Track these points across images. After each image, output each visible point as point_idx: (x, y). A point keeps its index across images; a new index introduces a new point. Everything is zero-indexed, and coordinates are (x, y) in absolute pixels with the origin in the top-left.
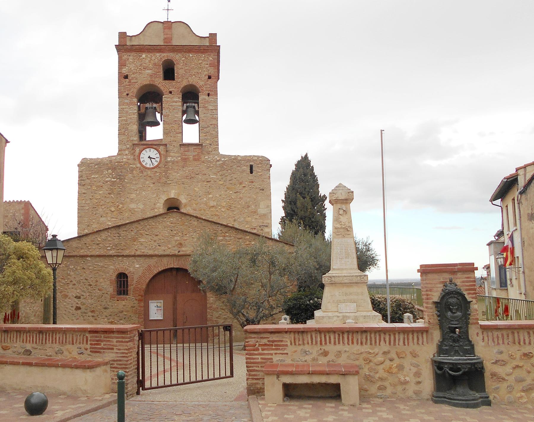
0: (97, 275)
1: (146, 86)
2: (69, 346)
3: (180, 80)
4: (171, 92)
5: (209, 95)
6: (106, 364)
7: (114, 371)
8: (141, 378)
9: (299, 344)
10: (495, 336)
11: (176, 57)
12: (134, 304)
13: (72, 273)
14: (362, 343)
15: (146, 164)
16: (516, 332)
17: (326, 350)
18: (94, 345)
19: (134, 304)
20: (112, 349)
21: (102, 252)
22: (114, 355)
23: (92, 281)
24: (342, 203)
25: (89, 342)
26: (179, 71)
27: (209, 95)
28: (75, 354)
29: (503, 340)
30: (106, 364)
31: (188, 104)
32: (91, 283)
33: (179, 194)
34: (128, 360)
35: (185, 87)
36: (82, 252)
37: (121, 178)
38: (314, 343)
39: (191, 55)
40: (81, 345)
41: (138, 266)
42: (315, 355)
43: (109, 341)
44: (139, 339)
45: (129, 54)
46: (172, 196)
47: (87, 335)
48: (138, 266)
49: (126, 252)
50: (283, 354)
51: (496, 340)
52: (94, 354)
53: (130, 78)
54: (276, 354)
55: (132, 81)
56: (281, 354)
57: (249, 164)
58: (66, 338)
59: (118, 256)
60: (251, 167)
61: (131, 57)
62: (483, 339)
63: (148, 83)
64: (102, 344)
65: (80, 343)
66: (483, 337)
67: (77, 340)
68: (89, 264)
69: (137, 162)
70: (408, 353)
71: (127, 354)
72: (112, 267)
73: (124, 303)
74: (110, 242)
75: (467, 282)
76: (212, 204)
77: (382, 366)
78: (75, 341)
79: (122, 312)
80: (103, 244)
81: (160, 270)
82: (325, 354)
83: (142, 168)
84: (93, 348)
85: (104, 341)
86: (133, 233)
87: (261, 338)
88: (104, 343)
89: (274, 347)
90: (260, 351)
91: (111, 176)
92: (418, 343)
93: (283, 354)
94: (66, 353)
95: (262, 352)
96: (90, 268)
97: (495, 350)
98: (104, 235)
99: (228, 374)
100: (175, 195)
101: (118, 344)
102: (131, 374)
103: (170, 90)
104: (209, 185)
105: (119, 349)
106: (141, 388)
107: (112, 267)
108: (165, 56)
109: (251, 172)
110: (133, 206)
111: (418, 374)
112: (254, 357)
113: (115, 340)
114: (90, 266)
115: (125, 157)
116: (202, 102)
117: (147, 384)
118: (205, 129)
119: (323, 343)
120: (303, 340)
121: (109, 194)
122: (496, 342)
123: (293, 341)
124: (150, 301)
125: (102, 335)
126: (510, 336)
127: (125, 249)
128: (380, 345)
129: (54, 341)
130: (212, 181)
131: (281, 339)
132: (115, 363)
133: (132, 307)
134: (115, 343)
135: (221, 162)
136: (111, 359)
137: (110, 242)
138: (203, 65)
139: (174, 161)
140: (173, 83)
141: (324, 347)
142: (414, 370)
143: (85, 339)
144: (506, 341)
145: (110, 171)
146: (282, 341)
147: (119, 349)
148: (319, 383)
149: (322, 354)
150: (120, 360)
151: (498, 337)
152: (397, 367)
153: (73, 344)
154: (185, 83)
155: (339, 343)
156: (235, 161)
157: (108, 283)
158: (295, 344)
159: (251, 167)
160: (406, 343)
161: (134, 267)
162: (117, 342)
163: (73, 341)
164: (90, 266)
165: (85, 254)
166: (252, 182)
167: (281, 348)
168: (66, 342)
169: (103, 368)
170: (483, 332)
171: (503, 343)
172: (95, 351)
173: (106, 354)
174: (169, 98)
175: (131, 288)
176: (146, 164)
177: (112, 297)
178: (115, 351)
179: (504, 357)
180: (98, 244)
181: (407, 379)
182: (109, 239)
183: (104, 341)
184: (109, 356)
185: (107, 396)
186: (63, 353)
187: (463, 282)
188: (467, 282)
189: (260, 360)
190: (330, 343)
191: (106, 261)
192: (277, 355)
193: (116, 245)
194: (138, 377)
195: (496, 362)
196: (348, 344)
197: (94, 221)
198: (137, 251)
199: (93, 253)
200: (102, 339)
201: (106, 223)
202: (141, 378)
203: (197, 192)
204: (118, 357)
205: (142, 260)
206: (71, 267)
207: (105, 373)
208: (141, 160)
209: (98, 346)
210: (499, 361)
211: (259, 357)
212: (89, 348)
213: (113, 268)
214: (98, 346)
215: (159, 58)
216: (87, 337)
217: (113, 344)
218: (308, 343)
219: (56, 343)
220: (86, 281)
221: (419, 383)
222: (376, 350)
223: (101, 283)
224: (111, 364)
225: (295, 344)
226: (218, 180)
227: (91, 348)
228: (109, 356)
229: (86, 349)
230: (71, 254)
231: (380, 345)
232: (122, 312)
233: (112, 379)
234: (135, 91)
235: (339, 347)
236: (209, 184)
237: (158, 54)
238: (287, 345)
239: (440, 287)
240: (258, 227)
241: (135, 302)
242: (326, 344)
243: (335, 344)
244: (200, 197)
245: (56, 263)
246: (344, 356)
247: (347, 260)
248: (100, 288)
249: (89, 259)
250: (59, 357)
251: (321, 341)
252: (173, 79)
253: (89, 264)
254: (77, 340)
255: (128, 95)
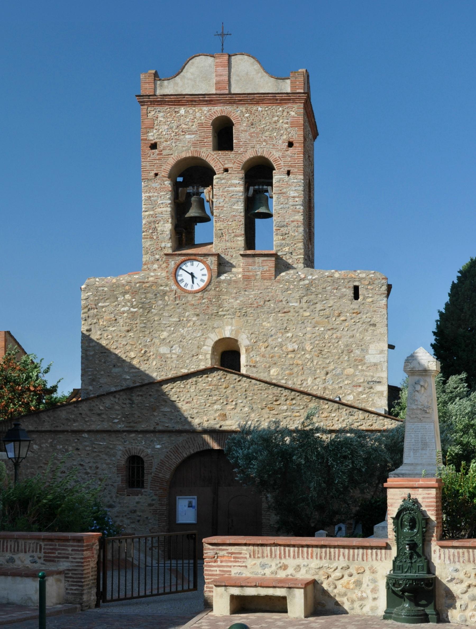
0: (98, 458)
1: (186, 159)
2: (21, 555)
3: (242, 150)
4: (226, 170)
5: (289, 173)
6: (59, 573)
7: (68, 581)
8: (101, 590)
9: (258, 557)
10: (451, 554)
11: (235, 113)
12: (153, 500)
13: (60, 456)
14: (321, 558)
15: (186, 285)
16: (471, 550)
17: (286, 563)
18: (49, 553)
19: (153, 500)
20: (68, 558)
21: (106, 426)
22: (69, 564)
23: (90, 467)
24: (420, 375)
25: (43, 551)
26: (240, 135)
27: (289, 173)
28: (27, 562)
29: (459, 558)
30: (59, 573)
31: (257, 187)
32: (89, 471)
33: (237, 332)
34: (84, 570)
35: (251, 160)
36: (76, 426)
37: (146, 307)
38: (273, 556)
39: (260, 109)
40: (34, 554)
41: (158, 446)
42: (274, 568)
43: (63, 549)
44: (100, 550)
45: (159, 108)
46: (227, 335)
47: (41, 543)
48: (158, 446)
49: (143, 427)
50: (241, 566)
51: (452, 557)
52: (48, 564)
53: (160, 147)
54: (234, 566)
55: (164, 153)
56: (239, 566)
57: (351, 285)
58: (18, 546)
59: (130, 432)
60: (356, 289)
61: (161, 114)
62: (440, 557)
63: (189, 155)
64: (57, 552)
65: (33, 551)
66: (440, 554)
67: (29, 548)
68: (86, 443)
69: (172, 282)
70: (367, 569)
71: (82, 563)
72: (120, 447)
73: (137, 498)
74: (117, 412)
75: (428, 498)
76: (290, 348)
77: (342, 581)
78: (27, 550)
79: (135, 511)
80: (107, 415)
81: (192, 452)
82: (285, 567)
83: (179, 291)
84: (47, 557)
85: (59, 549)
86: (152, 400)
87: (220, 550)
88: (59, 551)
89: (232, 560)
90: (219, 563)
91: (129, 304)
92: (376, 559)
93: (241, 566)
94: (18, 562)
95: (220, 564)
96: (88, 448)
97: (451, 569)
98: (108, 402)
99: (191, 587)
100: (231, 334)
101: (73, 552)
102: (88, 585)
103: (226, 166)
104: (287, 318)
105: (75, 558)
106: (101, 601)
107: (120, 447)
108: (218, 110)
109: (356, 297)
110: (164, 350)
111: (374, 590)
112: (212, 569)
113: (70, 549)
114: (87, 446)
115: (152, 274)
116: (277, 184)
117: (109, 597)
118: (282, 229)
119: (283, 557)
120: (263, 553)
121: (128, 331)
122: (452, 560)
123: (252, 554)
124: (178, 497)
125: (57, 544)
126: (466, 554)
127: (140, 422)
128: (338, 560)
129: (5, 550)
130: (292, 310)
131: (240, 552)
132: (70, 572)
133: (150, 505)
134: (70, 552)
135: (307, 282)
136: (66, 568)
137: (117, 412)
138: (279, 125)
139: (230, 280)
140: (231, 155)
141: (283, 561)
142: (372, 586)
143: (38, 547)
144: (461, 560)
145: (128, 297)
146: (241, 553)
147: (75, 558)
148: (266, 596)
149: (281, 567)
150: (75, 570)
151: (454, 555)
152: (354, 582)
153: (25, 552)
154: (250, 154)
155: (298, 557)
156: (329, 279)
157: (114, 470)
158: (254, 557)
159: (356, 289)
160: (365, 559)
161: (154, 448)
162: (72, 550)
163: (25, 549)
164: (87, 446)
165: (80, 428)
166: (358, 313)
167: (240, 560)
168: (18, 550)
169: (57, 577)
170: (440, 550)
171: (459, 561)
172: (48, 560)
173: (61, 564)
174: (224, 179)
175: (148, 478)
176: (186, 285)
177: (120, 491)
178: (71, 559)
179: (461, 575)
180: (99, 415)
181: (364, 595)
182: (117, 407)
183: (59, 549)
184: (64, 565)
185: (60, 606)
186: (14, 561)
187: (424, 498)
188: (428, 498)
189: (218, 572)
190: (289, 556)
191: (112, 440)
192: (236, 567)
193: (126, 417)
194: (98, 588)
195: (452, 580)
196: (307, 558)
197: (102, 372)
198: (158, 424)
199: (93, 427)
200: (57, 547)
201: (121, 376)
202: (101, 590)
203: (268, 329)
204: (73, 566)
205: (165, 438)
206: (58, 447)
207: (59, 583)
208: (179, 278)
209: (53, 555)
210: (454, 579)
211: (218, 569)
212: (42, 557)
213: (121, 449)
214: (53, 555)
215: (207, 114)
216: (40, 546)
217: (67, 552)
218: (267, 556)
219: (7, 551)
220: (81, 468)
221: (375, 599)
222: (334, 565)
223: (103, 470)
224: (66, 574)
225: (254, 557)
226: (301, 310)
227: (44, 557)
228: (64, 565)
229: (40, 558)
230: (59, 429)
231: (338, 560)
232: (135, 511)
233: (67, 589)
234: (169, 168)
235: (299, 561)
236: (287, 316)
237: (205, 109)
238: (245, 558)
239: (400, 502)
240: (366, 384)
241: (155, 497)
242: (285, 557)
243: (294, 557)
244: (272, 336)
245: (19, 458)
246: (303, 571)
247: (424, 452)
248: (102, 477)
249: (86, 435)
250: (11, 566)
251: (280, 554)
252: (230, 148)
253: (86, 443)
254: (29, 548)
255: (156, 175)
